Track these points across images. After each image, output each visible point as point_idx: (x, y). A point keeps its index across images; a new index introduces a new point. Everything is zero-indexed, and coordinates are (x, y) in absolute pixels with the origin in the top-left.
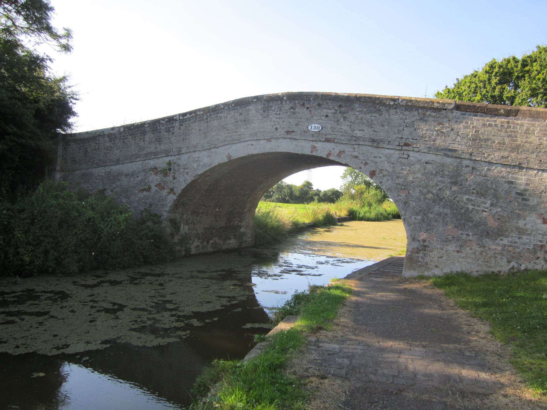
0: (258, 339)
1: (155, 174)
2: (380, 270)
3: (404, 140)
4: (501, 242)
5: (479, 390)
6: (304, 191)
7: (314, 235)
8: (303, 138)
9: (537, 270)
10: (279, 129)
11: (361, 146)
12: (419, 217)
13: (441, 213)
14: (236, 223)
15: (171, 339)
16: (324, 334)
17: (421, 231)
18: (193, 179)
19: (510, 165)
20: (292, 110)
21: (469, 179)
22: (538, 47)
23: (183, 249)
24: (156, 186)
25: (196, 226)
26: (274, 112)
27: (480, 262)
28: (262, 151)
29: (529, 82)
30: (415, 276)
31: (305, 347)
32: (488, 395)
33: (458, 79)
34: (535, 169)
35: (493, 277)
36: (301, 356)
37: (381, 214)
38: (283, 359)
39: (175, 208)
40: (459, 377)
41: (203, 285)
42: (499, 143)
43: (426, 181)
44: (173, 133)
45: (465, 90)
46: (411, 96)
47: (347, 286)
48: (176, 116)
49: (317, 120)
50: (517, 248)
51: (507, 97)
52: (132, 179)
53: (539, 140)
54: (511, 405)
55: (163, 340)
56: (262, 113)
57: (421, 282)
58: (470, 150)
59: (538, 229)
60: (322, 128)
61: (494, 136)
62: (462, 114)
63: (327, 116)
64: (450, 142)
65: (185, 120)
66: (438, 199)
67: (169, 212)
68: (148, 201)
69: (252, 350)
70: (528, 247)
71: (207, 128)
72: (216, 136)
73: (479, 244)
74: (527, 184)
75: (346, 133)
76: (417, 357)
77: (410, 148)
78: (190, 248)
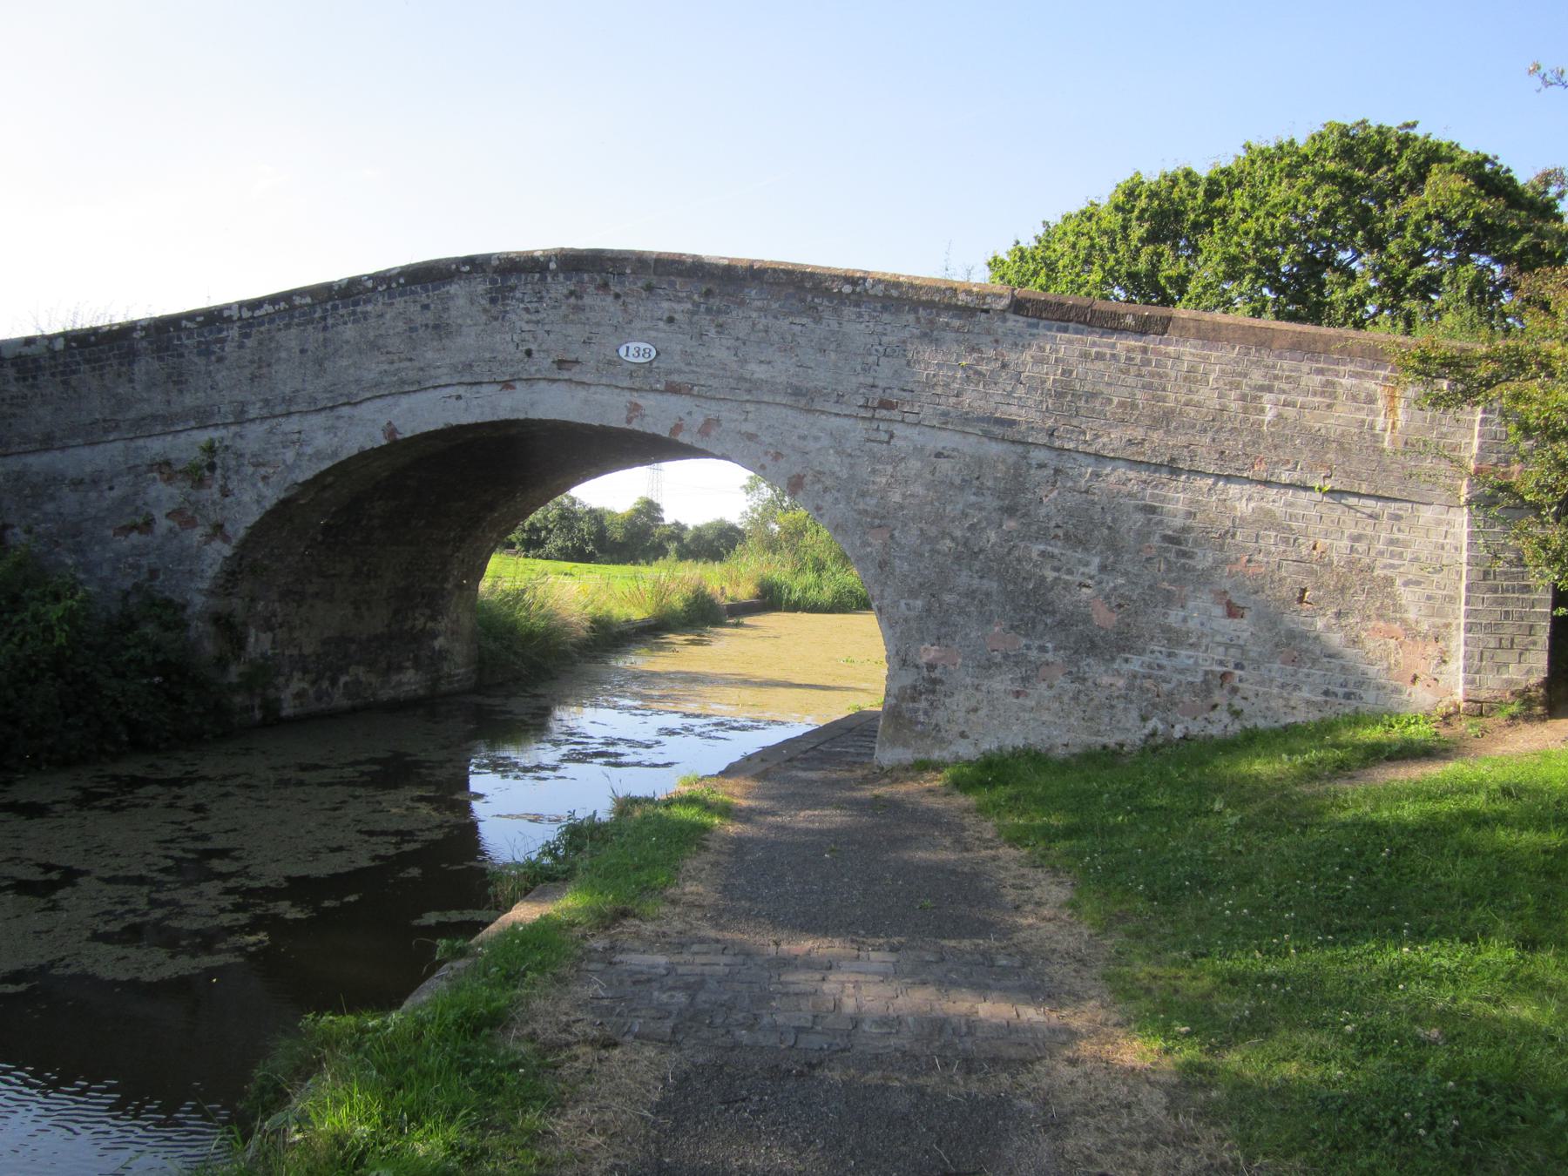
0: (446, 951)
1: (165, 481)
2: (821, 748)
3: (879, 392)
4: (1126, 667)
5: (1013, 1052)
6: (639, 527)
7: (656, 653)
8: (604, 381)
9: (1212, 736)
10: (535, 355)
11: (763, 406)
12: (919, 603)
13: (974, 592)
14: (420, 623)
15: (216, 958)
16: (633, 929)
17: (923, 640)
18: (282, 496)
19: (1148, 463)
20: (572, 300)
21: (1045, 500)
22: (1248, 147)
23: (257, 701)
24: (168, 515)
25: (296, 634)
26: (522, 306)
27: (1072, 720)
28: (488, 417)
29: (1222, 239)
30: (905, 763)
31: (573, 965)
32: (1032, 1063)
33: (1046, 224)
34: (1209, 475)
35: (1104, 758)
36: (559, 990)
37: (850, 592)
38: (503, 1002)
39: (228, 581)
40: (967, 1020)
41: (323, 803)
42: (1122, 405)
43: (936, 504)
45: (1063, 255)
46: (898, 271)
47: (721, 796)
48: (228, 307)
49: (643, 330)
50: (1165, 681)
51: (1168, 279)
52: (93, 495)
53: (1219, 398)
54: (1081, 1084)
55: (194, 962)
56: (488, 306)
57: (922, 778)
58: (1050, 423)
59: (1215, 632)
60: (658, 354)
61: (1109, 384)
62: (1030, 325)
63: (671, 320)
64: (998, 399)
65: (260, 321)
66: (968, 553)
67: (211, 593)
68: (144, 562)
69: (427, 983)
70: (1190, 679)
71: (326, 347)
72: (352, 371)
73: (1070, 673)
74: (1190, 515)
75: (724, 369)
76: (869, 978)
77: (895, 414)
78: (279, 700)
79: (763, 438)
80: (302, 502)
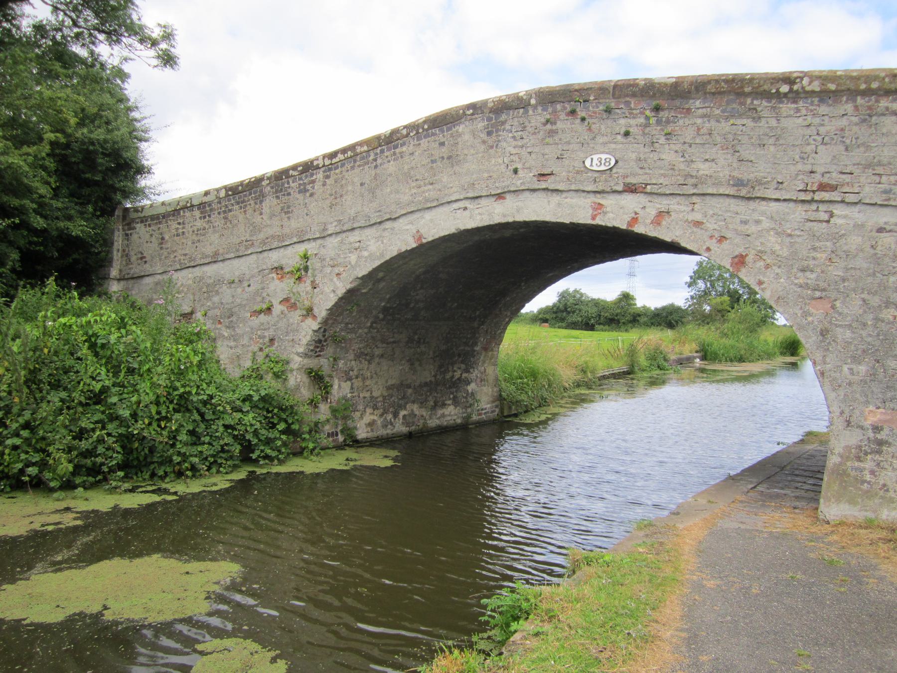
8: (573, 187)
10: (520, 172)
18: (349, 286)
20: (549, 126)
26: (510, 135)
44: (312, 195)
60: (617, 162)
63: (627, 134)
67: (306, 355)
79: (708, 225)
80: (364, 291)
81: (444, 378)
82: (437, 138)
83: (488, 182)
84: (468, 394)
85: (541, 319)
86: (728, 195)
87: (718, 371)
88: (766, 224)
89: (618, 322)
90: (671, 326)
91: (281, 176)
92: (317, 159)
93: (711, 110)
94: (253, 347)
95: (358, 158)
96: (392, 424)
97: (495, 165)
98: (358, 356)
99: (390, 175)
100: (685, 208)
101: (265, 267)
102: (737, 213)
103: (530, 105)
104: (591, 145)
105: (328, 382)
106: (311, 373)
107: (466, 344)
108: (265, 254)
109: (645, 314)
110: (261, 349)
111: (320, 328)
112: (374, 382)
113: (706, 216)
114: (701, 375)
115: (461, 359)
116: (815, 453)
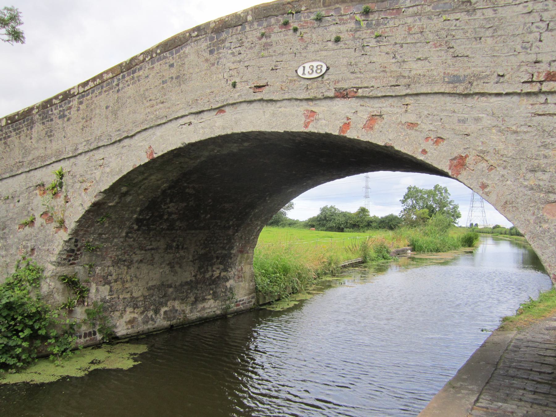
8: (286, 96)
10: (238, 85)
18: (94, 200)
20: (264, 40)
26: (230, 51)
44: (69, 120)
60: (328, 68)
63: (337, 40)
67: (59, 264)
79: (423, 126)
80: (110, 204)
81: (204, 277)
82: (168, 61)
83: (210, 97)
84: (226, 289)
85: (310, 225)
86: (443, 94)
87: (423, 259)
88: (487, 121)
89: (359, 226)
90: (391, 228)
91: (47, 104)
92: (74, 88)
93: (422, 8)
94: (18, 256)
95: (105, 84)
96: (152, 319)
97: (216, 81)
98: (116, 262)
99: (130, 97)
100: (399, 110)
101: (31, 185)
102: (454, 112)
103: (247, 21)
104: (304, 55)
105: (83, 287)
106: (64, 279)
107: (223, 248)
108: (32, 173)
109: (375, 221)
110: (24, 258)
111: (70, 239)
112: (134, 284)
113: (420, 117)
114: (412, 262)
115: (219, 261)
116: (519, 343)
